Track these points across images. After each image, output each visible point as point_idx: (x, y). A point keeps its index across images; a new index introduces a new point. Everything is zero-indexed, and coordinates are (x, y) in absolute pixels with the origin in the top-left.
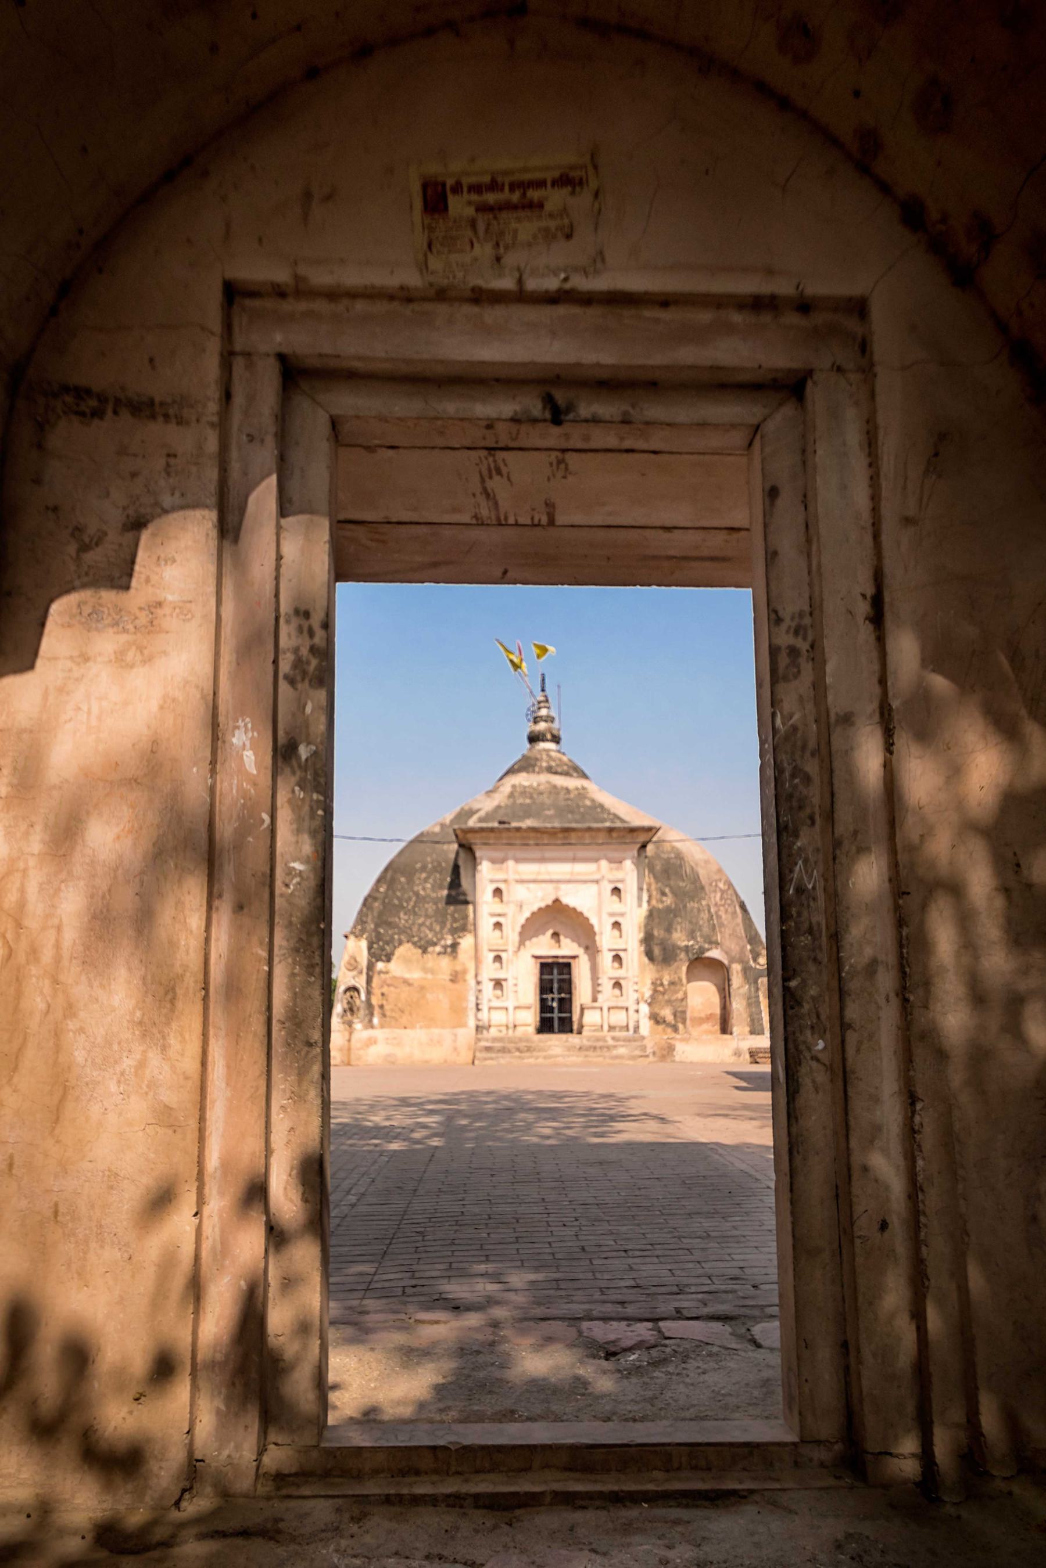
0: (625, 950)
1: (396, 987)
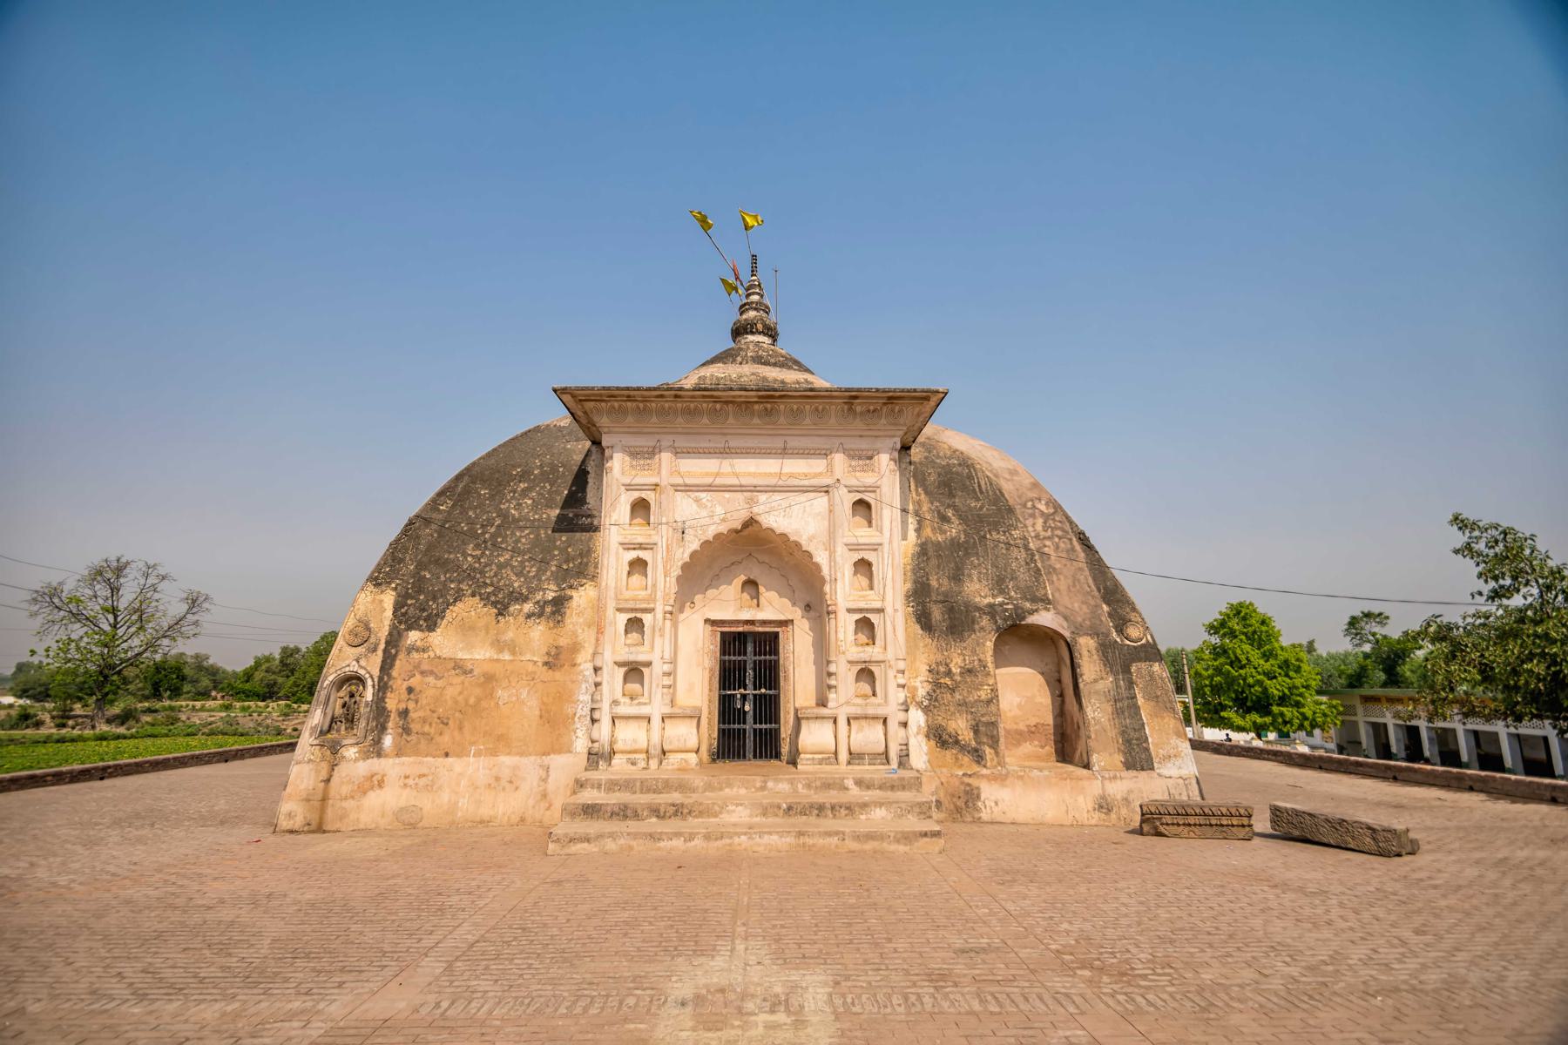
0: (881, 611)
1: (438, 678)
